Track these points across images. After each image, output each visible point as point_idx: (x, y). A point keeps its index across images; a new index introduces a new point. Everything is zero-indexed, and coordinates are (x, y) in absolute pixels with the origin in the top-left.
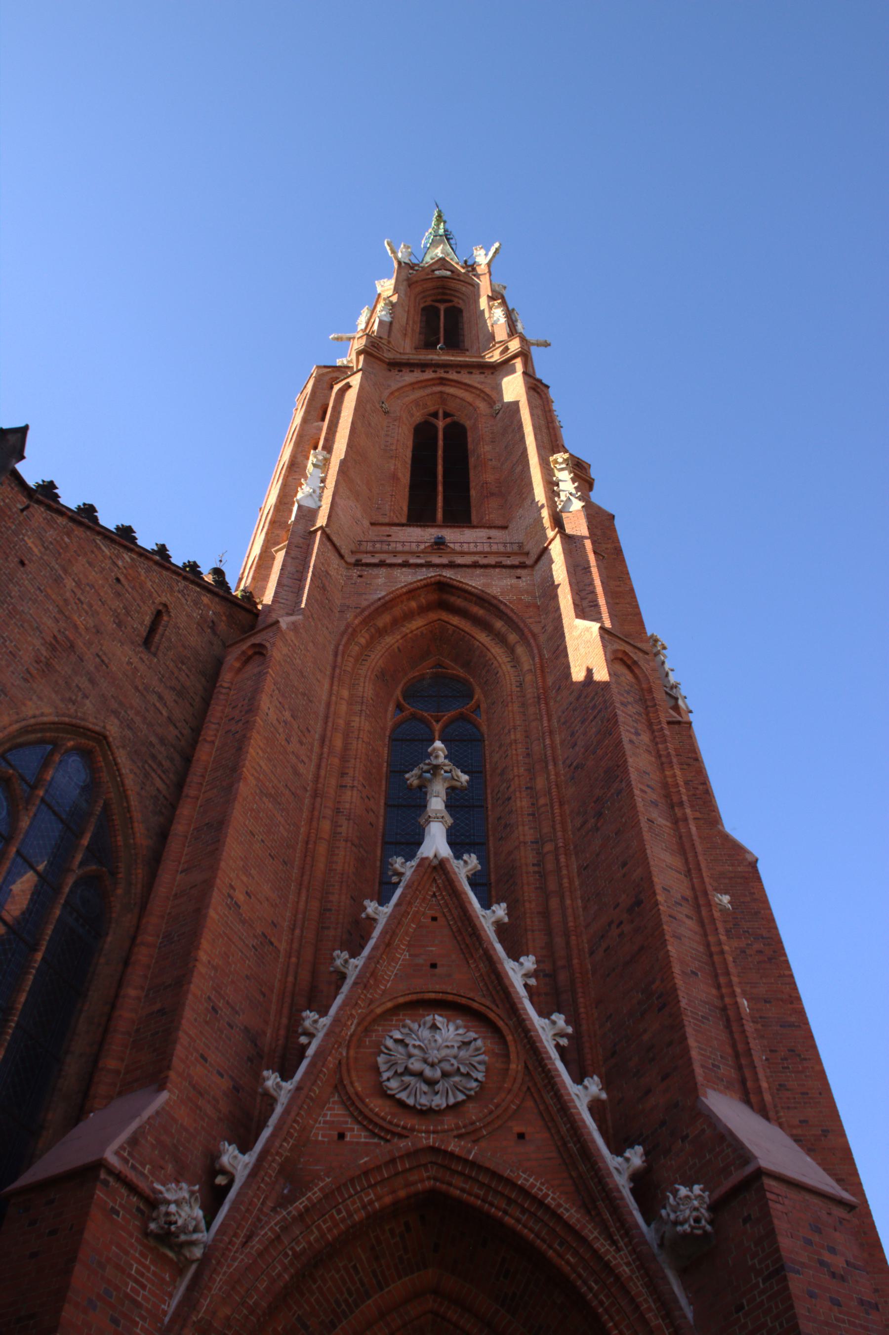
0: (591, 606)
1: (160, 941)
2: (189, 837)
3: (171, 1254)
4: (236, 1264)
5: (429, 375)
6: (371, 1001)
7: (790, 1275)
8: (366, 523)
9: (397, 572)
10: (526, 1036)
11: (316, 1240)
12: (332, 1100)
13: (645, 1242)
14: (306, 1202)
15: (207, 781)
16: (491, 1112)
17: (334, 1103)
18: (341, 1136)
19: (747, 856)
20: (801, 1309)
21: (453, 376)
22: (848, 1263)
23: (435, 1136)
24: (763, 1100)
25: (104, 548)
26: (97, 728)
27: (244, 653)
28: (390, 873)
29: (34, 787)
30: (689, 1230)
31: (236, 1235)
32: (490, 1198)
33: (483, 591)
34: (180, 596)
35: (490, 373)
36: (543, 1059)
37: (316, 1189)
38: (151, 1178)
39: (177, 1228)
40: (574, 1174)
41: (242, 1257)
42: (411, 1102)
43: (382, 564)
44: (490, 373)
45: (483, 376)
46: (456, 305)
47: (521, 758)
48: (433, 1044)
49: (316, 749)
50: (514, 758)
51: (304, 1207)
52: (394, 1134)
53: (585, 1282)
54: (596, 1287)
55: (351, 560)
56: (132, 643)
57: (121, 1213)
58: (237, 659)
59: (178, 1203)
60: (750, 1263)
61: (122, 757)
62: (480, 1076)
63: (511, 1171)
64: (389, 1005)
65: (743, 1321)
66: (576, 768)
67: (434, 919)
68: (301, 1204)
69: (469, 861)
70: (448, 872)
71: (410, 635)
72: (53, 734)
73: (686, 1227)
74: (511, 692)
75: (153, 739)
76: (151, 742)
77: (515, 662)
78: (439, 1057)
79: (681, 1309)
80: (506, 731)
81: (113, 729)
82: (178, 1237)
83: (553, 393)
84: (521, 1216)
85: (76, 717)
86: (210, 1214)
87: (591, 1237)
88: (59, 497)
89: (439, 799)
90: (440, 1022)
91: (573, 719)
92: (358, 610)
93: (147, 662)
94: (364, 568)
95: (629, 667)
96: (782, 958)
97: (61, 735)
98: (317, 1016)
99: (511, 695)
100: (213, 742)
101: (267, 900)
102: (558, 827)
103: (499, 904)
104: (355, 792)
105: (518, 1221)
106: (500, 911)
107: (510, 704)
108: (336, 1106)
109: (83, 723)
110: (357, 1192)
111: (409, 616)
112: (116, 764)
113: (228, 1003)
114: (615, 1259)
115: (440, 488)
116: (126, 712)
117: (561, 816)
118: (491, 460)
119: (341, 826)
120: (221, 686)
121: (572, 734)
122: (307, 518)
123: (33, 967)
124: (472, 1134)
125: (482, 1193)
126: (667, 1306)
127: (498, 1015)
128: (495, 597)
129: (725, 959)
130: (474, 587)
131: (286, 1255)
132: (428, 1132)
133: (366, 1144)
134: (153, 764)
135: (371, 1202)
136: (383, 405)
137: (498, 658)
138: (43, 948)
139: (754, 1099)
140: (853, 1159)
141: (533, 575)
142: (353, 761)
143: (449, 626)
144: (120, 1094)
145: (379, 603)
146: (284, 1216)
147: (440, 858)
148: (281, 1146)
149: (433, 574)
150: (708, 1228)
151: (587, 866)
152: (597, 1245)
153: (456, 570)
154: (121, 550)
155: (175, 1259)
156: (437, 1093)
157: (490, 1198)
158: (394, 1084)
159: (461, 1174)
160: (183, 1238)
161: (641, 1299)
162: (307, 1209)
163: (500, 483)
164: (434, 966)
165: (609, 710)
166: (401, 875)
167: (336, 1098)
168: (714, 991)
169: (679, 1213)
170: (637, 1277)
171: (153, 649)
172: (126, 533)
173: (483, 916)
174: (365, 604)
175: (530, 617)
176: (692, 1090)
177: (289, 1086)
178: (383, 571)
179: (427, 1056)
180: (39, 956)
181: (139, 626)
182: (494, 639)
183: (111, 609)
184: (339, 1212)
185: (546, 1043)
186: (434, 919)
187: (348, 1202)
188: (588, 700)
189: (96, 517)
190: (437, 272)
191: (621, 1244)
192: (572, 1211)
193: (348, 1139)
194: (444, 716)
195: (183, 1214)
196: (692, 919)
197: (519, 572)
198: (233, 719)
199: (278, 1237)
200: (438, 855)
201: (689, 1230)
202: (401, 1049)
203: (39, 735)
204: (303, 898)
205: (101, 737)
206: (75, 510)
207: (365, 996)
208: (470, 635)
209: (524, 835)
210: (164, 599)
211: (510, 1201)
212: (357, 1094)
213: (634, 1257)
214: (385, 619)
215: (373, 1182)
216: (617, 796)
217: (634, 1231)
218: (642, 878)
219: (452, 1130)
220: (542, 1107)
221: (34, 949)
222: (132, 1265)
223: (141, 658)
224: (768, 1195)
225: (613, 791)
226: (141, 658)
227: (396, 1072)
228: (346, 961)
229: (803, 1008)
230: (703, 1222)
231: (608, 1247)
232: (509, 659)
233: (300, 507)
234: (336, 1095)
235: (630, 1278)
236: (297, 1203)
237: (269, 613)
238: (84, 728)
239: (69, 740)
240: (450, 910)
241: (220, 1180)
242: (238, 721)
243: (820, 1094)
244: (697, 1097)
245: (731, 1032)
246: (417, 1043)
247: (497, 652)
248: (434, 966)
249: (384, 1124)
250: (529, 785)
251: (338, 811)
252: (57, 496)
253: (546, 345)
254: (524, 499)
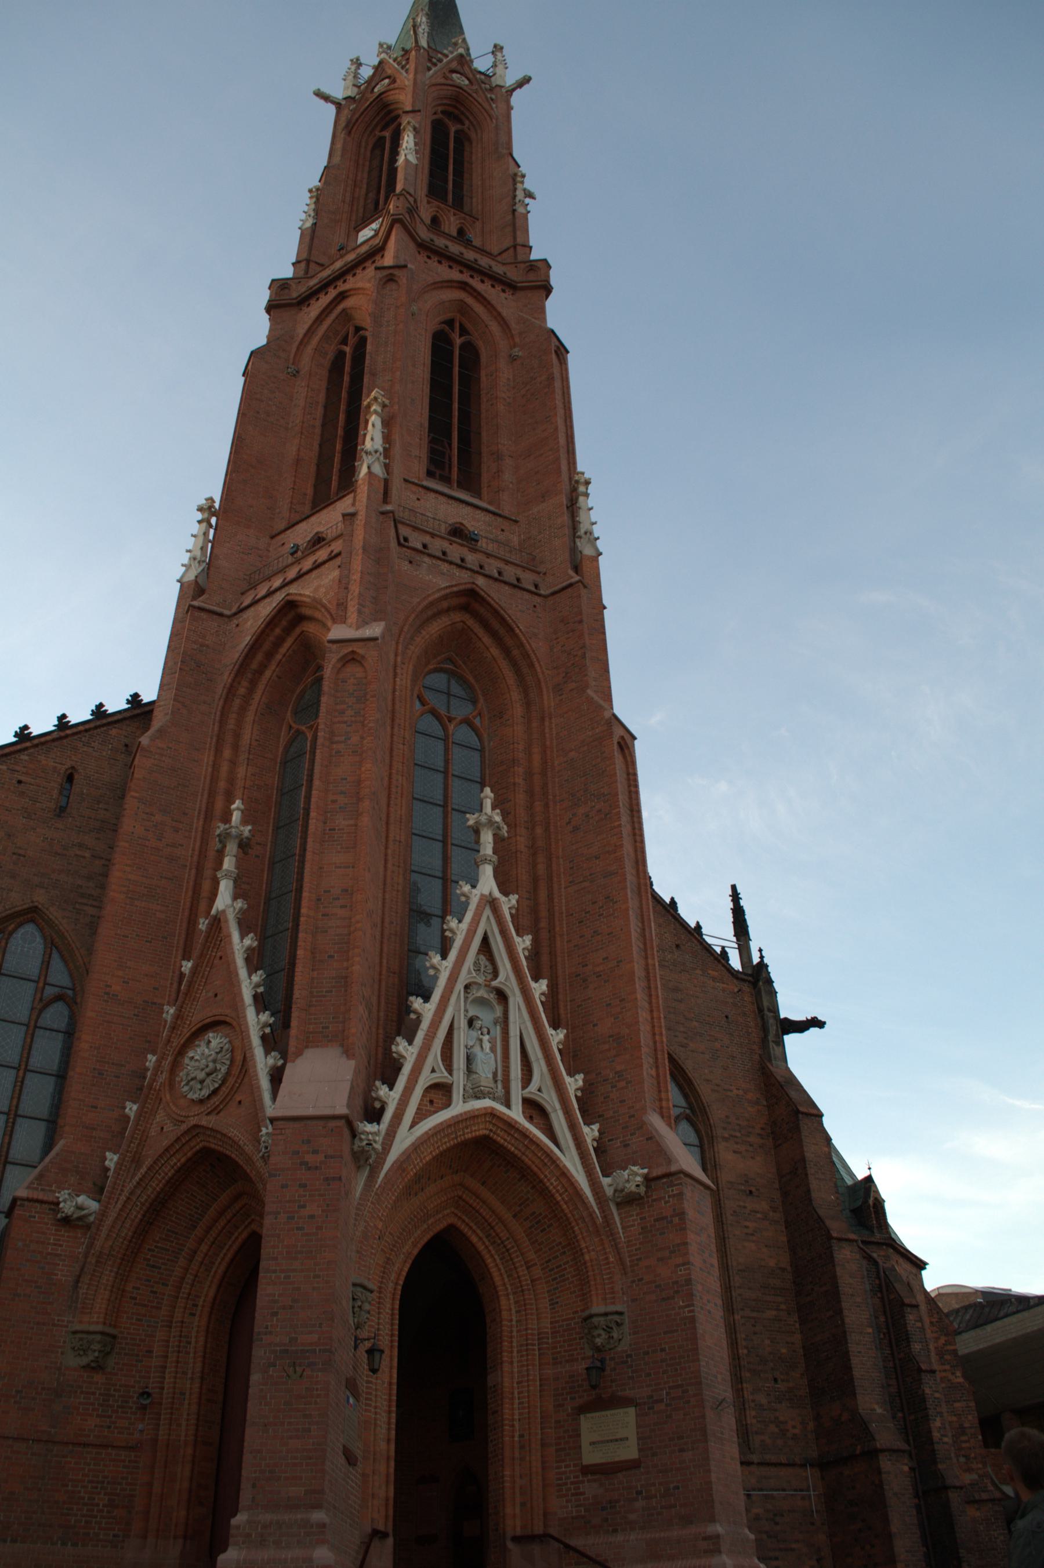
5: (324, 300)
11: (152, 1193)
21: (475, 283)
71: (284, 660)
105: (505, 1140)
164: (216, 995)
184: (160, 1174)
190: (376, 90)
206: (91, 717)
253: (319, 94)
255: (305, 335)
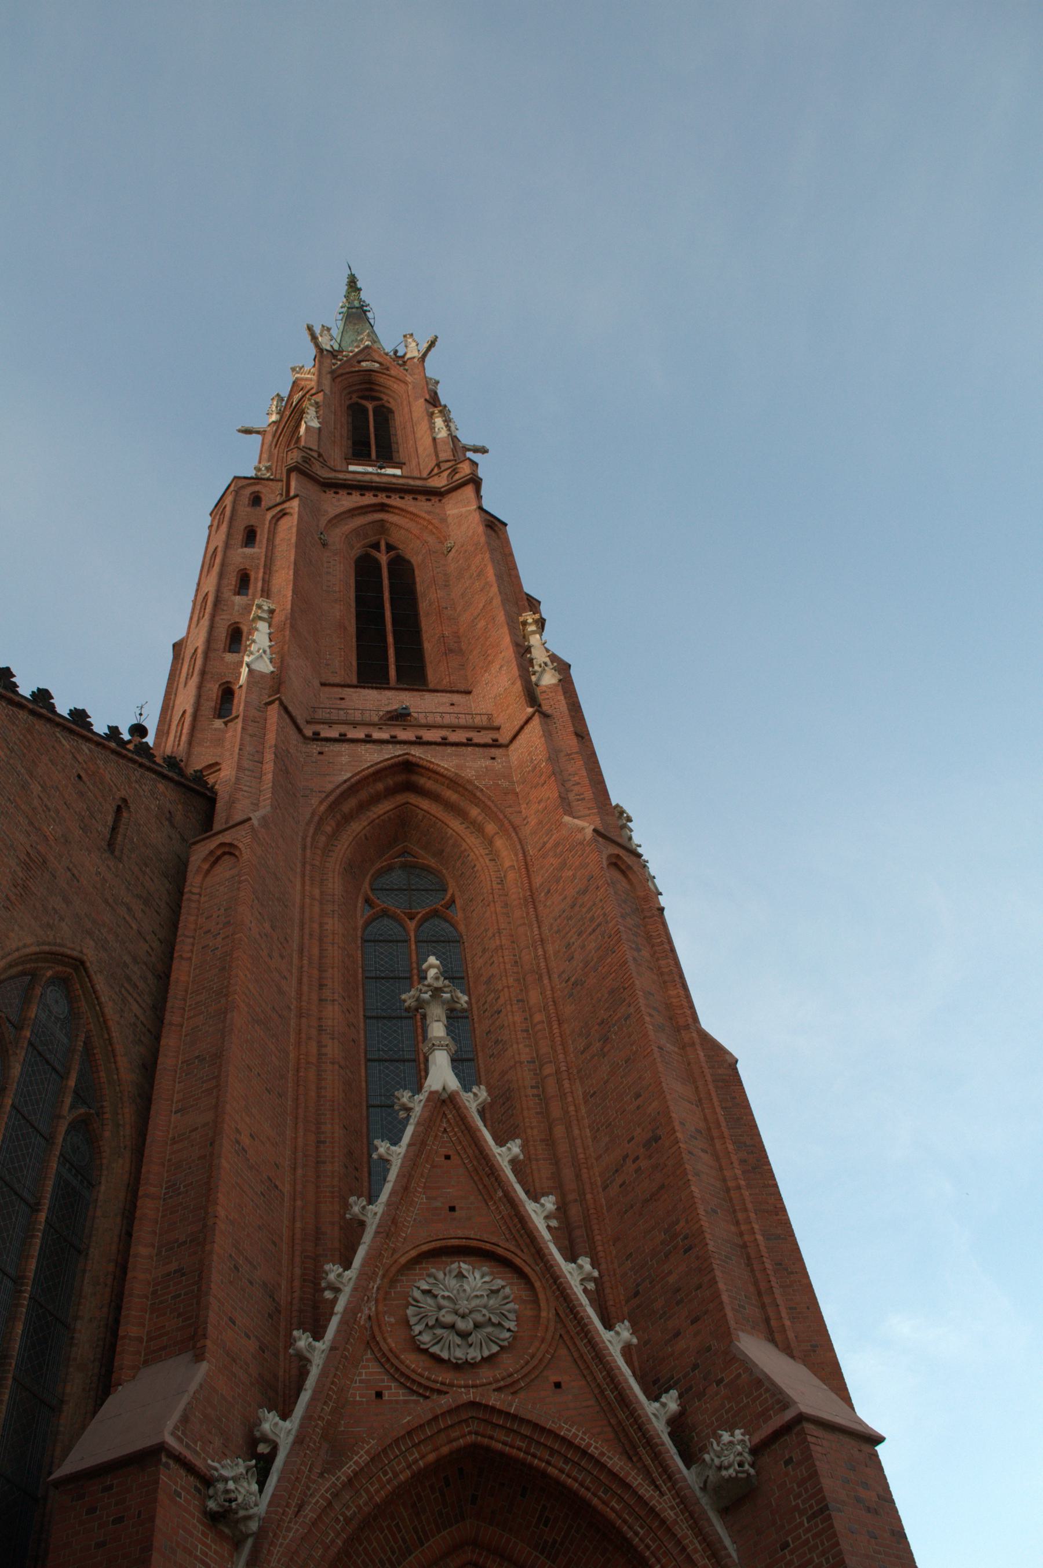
0: (578, 800)
1: (164, 1191)
2: (178, 1072)
3: (226, 1530)
4: (291, 1534)
5: (369, 499)
6: (394, 1251)
7: (833, 1514)
8: (316, 683)
9: (362, 749)
10: (555, 1282)
11: (366, 1504)
12: (364, 1357)
13: (689, 1487)
14: (354, 1467)
15: (190, 1006)
16: (527, 1363)
17: (368, 1360)
18: (379, 1395)
19: (727, 1057)
20: (845, 1545)
22: (879, 1496)
23: (475, 1390)
24: (787, 1338)
25: (63, 741)
26: (75, 954)
27: (212, 852)
28: (397, 1107)
29: (18, 1028)
30: (734, 1475)
31: (288, 1505)
32: (532, 1450)
33: (456, 774)
34: (137, 787)
35: (437, 500)
36: (574, 1307)
37: (362, 1452)
38: (203, 1455)
39: (238, 1505)
40: (613, 1421)
41: (297, 1526)
42: (445, 1355)
43: (342, 739)
44: (437, 500)
45: (429, 504)
46: (387, 404)
47: (508, 966)
48: (462, 1294)
49: (295, 961)
50: (502, 967)
51: (352, 1471)
52: (432, 1390)
53: (630, 1528)
54: (642, 1532)
55: (308, 732)
56: (99, 850)
57: (183, 1494)
58: (205, 860)
59: (235, 1479)
60: (793, 1503)
61: (101, 983)
62: (512, 1325)
63: (553, 1422)
64: (414, 1253)
65: (788, 1558)
66: (575, 984)
67: (448, 1157)
68: (349, 1468)
69: (479, 1094)
70: (460, 1108)
71: (377, 821)
72: (33, 965)
73: (731, 1471)
74: (492, 889)
75: (127, 958)
76: (125, 962)
77: (494, 856)
78: (470, 1307)
79: (725, 1548)
80: (490, 934)
81: (90, 953)
82: (237, 1513)
83: (513, 533)
84: (564, 1466)
85: (55, 944)
86: (261, 1484)
87: (635, 1485)
88: (18, 687)
89: (440, 1024)
90: (466, 1270)
91: (568, 929)
92: (323, 795)
93: (114, 869)
94: (324, 743)
95: (623, 872)
96: (766, 1167)
97: (40, 965)
98: (341, 1270)
99: (492, 893)
100: (190, 959)
101: (269, 1140)
102: (559, 1048)
103: (513, 1140)
104: (336, 1007)
105: (562, 1471)
106: (515, 1148)
107: (492, 904)
108: (370, 1364)
109: (61, 950)
110: (402, 1453)
111: (376, 799)
112: (95, 992)
113: (247, 1259)
114: (660, 1503)
115: (390, 639)
116: (99, 931)
117: (561, 1036)
118: (446, 608)
119: (326, 1046)
120: (191, 892)
121: (568, 946)
122: (260, 685)
123: (38, 1230)
124: (510, 1387)
125: (524, 1445)
126: (713, 1550)
127: (524, 1261)
128: (470, 782)
129: (742, 1195)
130: (446, 769)
131: (337, 1521)
132: (466, 1387)
133: (406, 1402)
134: (129, 988)
135: (416, 1461)
136: (322, 536)
137: (475, 850)
138: (46, 1207)
139: (778, 1337)
140: (841, 1374)
141: (508, 756)
142: (330, 970)
143: (419, 811)
144: (146, 1363)
145: (345, 786)
146: (333, 1482)
147: (449, 1092)
148: (323, 1409)
149: (400, 752)
150: (752, 1471)
151: (595, 1093)
152: (641, 1492)
153: (426, 748)
154: (80, 741)
155: (231, 1534)
156: (471, 1345)
157: (532, 1450)
158: (426, 1338)
159: (502, 1427)
160: (242, 1513)
161: (687, 1541)
162: (356, 1474)
163: (459, 637)
164: (452, 1209)
165: (611, 925)
166: (408, 1110)
167: (369, 1355)
168: (733, 1228)
169: (723, 1458)
170: (682, 1520)
171: (117, 853)
172: (80, 716)
173: (499, 1154)
174: (329, 787)
175: (510, 806)
176: (726, 1335)
177: (319, 1345)
178: (345, 747)
179: (457, 1307)
180: (43, 1216)
181: (103, 829)
182: (468, 827)
183: (76, 812)
184: (385, 1473)
185: (575, 1289)
186: (448, 1157)
187: (394, 1463)
188: (584, 910)
189: (53, 704)
190: (364, 364)
191: (664, 1488)
192: (616, 1459)
193: (386, 1397)
194: (418, 913)
195: (242, 1490)
196: (707, 1152)
197: (494, 752)
198: (209, 931)
199: (330, 1504)
200: (446, 1088)
201: (734, 1475)
202: (430, 1301)
203: (20, 968)
204: (301, 1133)
205: (78, 963)
207: (388, 1244)
208: (443, 822)
209: (519, 1054)
210: (123, 794)
211: (552, 1452)
212: (391, 1351)
213: (678, 1500)
214: (352, 803)
215: (417, 1441)
216: (626, 1021)
217: (677, 1476)
218: (658, 1113)
219: (490, 1384)
220: (576, 1355)
221: (35, 1208)
222: (197, 1546)
223: (108, 866)
224: (809, 1438)
225: (619, 1015)
226: (108, 866)
227: (427, 1325)
228: (364, 1208)
229: (788, 1219)
230: (747, 1467)
231: (652, 1492)
232: (487, 852)
233: (251, 671)
234: (369, 1352)
235: (675, 1522)
236: (345, 1468)
237: (234, 803)
238: (62, 955)
239: (50, 968)
240: (464, 1148)
241: (263, 1449)
242: (217, 935)
243: (808, 1308)
244: (731, 1341)
245: (752, 1271)
246: (446, 1294)
247: (472, 841)
248: (452, 1209)
249: (423, 1381)
250: (520, 997)
251: (320, 1029)
252: (15, 685)
254: (491, 662)
255: (336, 516)
